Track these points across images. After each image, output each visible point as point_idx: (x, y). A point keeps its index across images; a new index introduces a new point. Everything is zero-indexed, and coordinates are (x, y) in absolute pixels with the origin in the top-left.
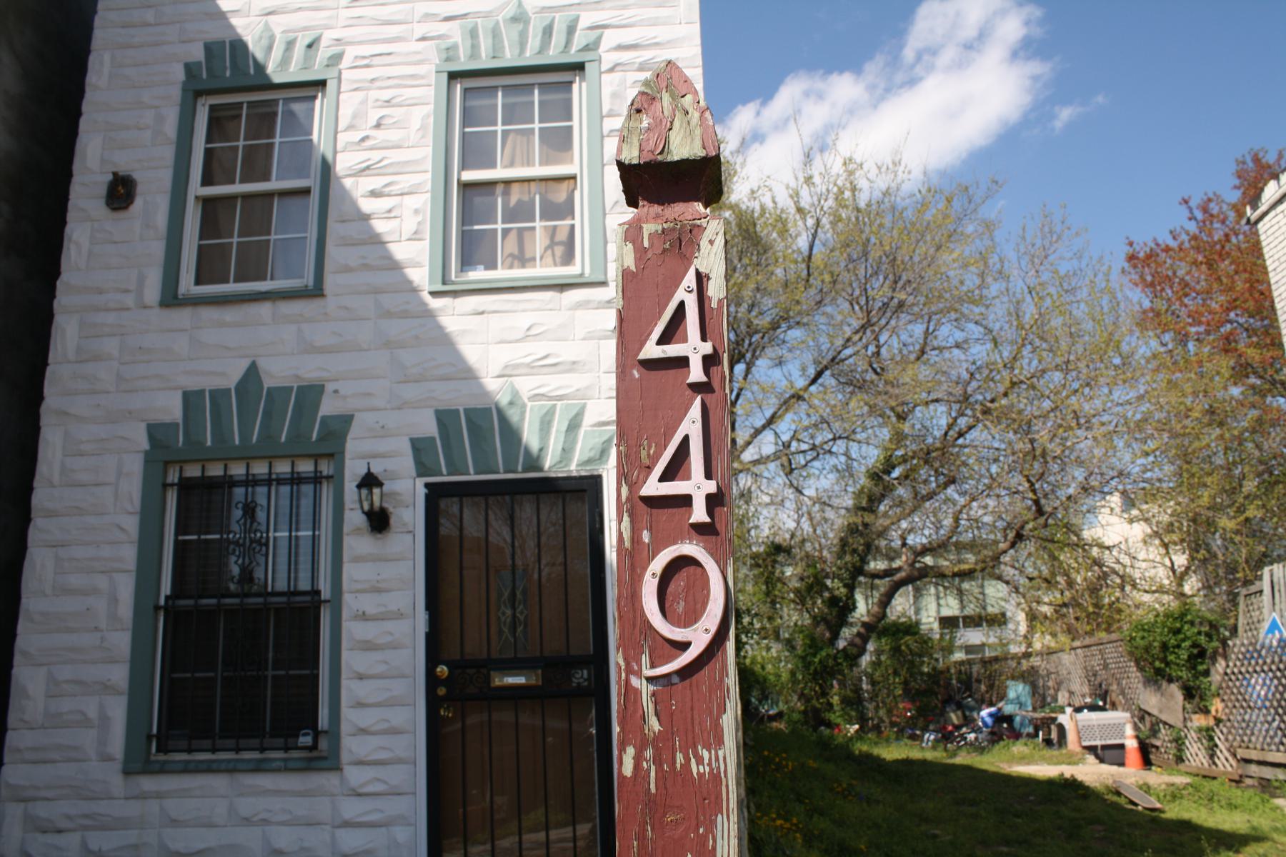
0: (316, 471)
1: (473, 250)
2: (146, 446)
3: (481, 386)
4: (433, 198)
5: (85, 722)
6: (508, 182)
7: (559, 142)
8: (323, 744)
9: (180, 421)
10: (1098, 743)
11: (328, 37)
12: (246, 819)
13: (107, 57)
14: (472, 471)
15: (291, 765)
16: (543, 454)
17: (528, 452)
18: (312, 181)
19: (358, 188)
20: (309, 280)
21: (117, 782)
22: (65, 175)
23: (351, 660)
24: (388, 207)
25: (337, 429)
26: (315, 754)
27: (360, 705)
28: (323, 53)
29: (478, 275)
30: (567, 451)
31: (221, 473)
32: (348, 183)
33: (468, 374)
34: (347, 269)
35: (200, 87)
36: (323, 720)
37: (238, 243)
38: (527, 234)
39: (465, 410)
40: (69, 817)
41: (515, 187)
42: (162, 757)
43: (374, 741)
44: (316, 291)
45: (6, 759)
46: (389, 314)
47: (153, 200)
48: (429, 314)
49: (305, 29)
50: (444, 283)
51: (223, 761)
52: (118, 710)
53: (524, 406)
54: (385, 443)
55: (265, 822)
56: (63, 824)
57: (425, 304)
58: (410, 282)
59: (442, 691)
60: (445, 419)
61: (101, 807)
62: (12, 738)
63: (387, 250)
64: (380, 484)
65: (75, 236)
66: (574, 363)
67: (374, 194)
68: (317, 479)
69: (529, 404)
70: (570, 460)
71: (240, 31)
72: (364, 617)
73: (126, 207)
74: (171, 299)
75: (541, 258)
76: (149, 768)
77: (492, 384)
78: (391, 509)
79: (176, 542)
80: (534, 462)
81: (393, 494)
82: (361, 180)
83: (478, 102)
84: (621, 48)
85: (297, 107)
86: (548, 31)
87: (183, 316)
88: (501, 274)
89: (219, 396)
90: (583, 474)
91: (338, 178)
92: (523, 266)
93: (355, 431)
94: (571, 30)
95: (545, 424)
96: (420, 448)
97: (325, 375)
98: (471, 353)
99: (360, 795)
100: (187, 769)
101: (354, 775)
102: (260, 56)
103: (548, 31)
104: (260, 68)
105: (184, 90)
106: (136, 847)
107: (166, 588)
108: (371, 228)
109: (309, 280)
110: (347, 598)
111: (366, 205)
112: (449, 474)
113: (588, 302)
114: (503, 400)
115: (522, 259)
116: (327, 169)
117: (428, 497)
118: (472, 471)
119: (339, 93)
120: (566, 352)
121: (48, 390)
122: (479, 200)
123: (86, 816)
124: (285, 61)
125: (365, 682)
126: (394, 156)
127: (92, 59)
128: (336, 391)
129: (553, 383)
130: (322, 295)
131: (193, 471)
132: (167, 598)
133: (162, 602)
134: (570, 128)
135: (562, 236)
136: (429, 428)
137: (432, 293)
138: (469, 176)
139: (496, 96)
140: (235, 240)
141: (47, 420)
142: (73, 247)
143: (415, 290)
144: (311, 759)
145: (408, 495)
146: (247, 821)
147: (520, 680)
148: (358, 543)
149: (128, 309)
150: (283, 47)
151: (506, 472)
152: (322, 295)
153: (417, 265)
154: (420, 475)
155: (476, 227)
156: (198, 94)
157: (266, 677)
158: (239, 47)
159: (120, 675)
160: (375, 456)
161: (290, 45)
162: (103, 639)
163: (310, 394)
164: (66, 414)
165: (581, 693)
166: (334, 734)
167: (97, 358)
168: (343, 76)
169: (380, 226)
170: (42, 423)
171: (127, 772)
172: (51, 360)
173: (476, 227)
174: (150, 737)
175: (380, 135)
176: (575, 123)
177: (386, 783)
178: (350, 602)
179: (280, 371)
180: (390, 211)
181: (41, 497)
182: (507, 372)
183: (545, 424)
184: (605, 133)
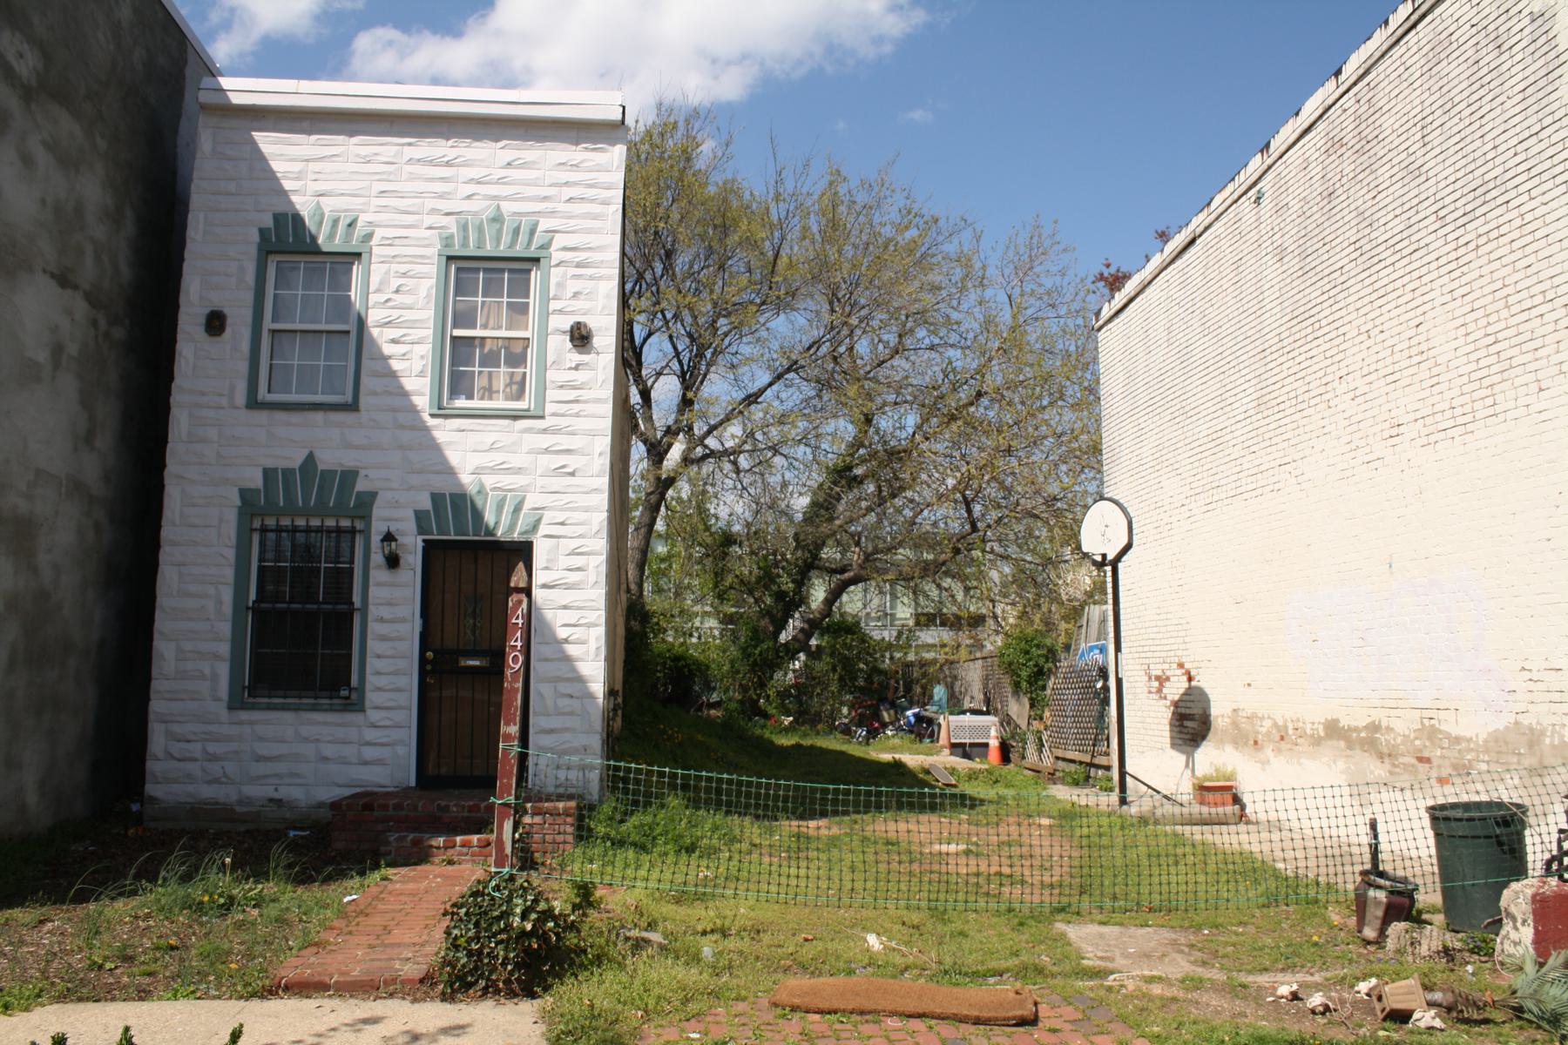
3: (458, 480)
6: (483, 338)
18: (352, 326)
19: (380, 335)
20: (349, 398)
21: (223, 713)
22: (175, 308)
23: (372, 645)
25: (366, 502)
27: (378, 673)
29: (461, 403)
32: (375, 332)
33: (450, 472)
34: (375, 393)
36: (354, 681)
43: (387, 695)
44: (353, 407)
46: (402, 427)
48: (426, 430)
52: (224, 670)
54: (397, 513)
55: (318, 740)
59: (429, 667)
60: (437, 499)
62: (155, 685)
67: (394, 341)
72: (381, 620)
76: (244, 707)
77: (466, 479)
80: (490, 533)
84: (565, 249)
86: (516, 231)
87: (262, 416)
88: (476, 403)
89: (288, 473)
93: (378, 503)
96: (420, 516)
101: (373, 715)
102: (313, 229)
103: (516, 231)
104: (314, 239)
105: (260, 250)
107: (253, 596)
109: (349, 398)
110: (372, 608)
111: (387, 349)
114: (472, 490)
115: (489, 392)
116: (361, 323)
120: (516, 461)
124: (331, 236)
126: (409, 315)
129: (506, 481)
135: (518, 378)
136: (426, 504)
142: (183, 362)
143: (413, 410)
147: (477, 663)
153: (422, 394)
154: (420, 533)
156: (270, 252)
158: (298, 220)
159: (225, 649)
161: (336, 222)
163: (349, 476)
166: (361, 690)
169: (395, 365)
171: (231, 708)
175: (399, 299)
178: (374, 611)
179: (329, 459)
181: (166, 532)
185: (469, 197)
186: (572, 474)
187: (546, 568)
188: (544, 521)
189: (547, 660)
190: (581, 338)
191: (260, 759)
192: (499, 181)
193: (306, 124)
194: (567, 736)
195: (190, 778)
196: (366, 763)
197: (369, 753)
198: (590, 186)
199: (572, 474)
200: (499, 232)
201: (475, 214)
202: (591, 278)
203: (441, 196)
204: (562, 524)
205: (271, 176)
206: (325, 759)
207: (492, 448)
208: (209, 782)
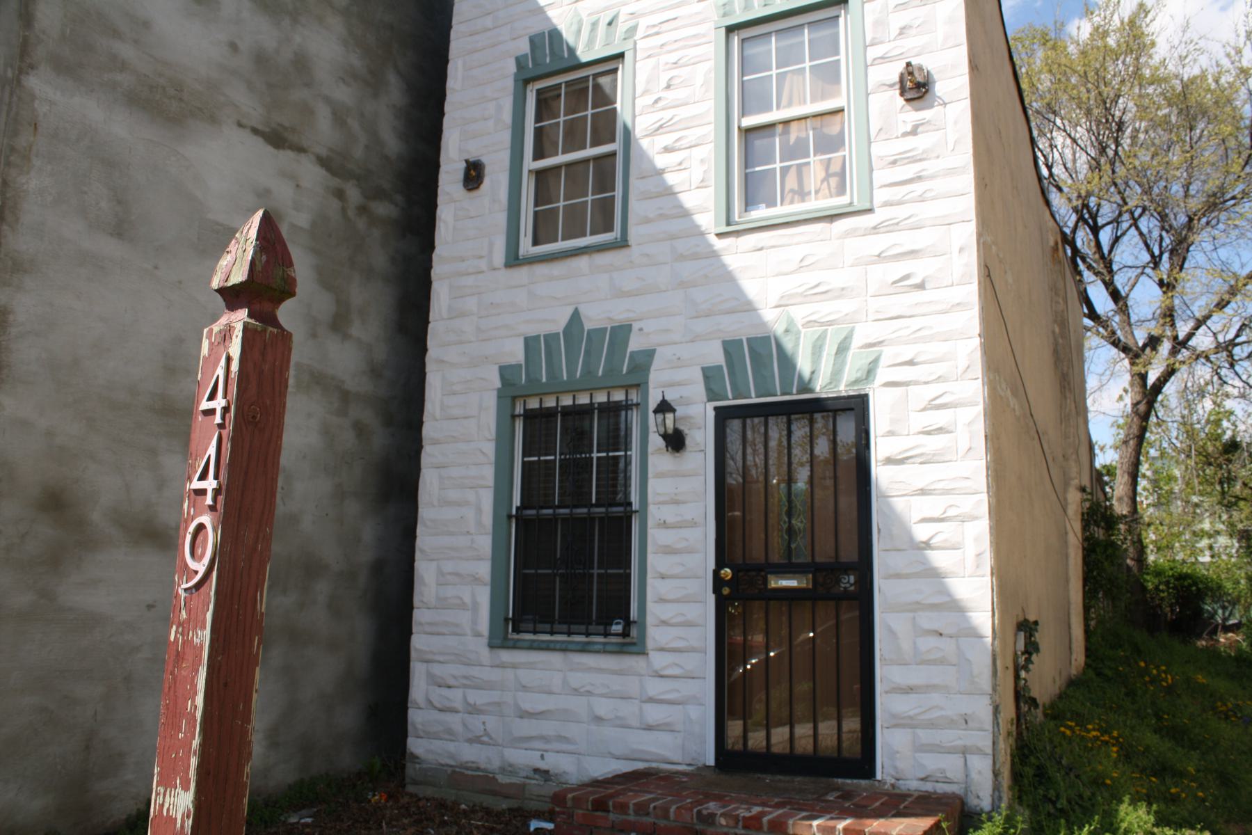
0: (627, 400)
2: (498, 384)
3: (759, 317)
4: (716, 147)
5: (462, 606)
6: (786, 123)
7: (829, 76)
8: (634, 632)
9: (523, 362)
11: (625, 11)
12: (576, 690)
13: (460, 63)
14: (753, 395)
15: (609, 648)
16: (815, 376)
17: (800, 377)
21: (485, 652)
23: (655, 562)
24: (678, 161)
25: (643, 362)
26: (627, 640)
27: (662, 600)
28: (621, 28)
29: (761, 213)
30: (836, 374)
31: (554, 404)
33: (748, 307)
34: (647, 221)
35: (529, 76)
36: (634, 613)
37: (564, 206)
38: (804, 169)
39: (748, 340)
40: (454, 677)
41: (794, 126)
42: (516, 636)
45: (414, 630)
46: (682, 258)
48: (714, 255)
49: (607, 8)
50: (728, 224)
51: (558, 642)
52: (484, 597)
53: (799, 332)
55: (589, 693)
56: (452, 682)
57: (711, 246)
58: (698, 227)
59: (726, 591)
61: (475, 672)
63: (677, 200)
64: (673, 411)
65: (443, 216)
66: (843, 289)
67: (667, 150)
68: (628, 406)
69: (803, 331)
70: (839, 381)
71: (555, 21)
72: (664, 525)
73: (477, 187)
74: (514, 260)
75: (817, 192)
78: (686, 431)
79: (524, 463)
80: (805, 387)
81: (686, 418)
82: (656, 138)
83: (754, 50)
85: (603, 81)
87: (522, 273)
89: (551, 339)
90: (852, 393)
91: (637, 140)
92: (803, 201)
95: (817, 350)
96: (710, 375)
97: (631, 315)
98: (751, 288)
99: (662, 676)
100: (532, 647)
101: (658, 660)
104: (572, 51)
106: (498, 704)
107: (517, 501)
108: (664, 181)
110: (652, 509)
111: (660, 161)
112: (734, 398)
113: (855, 230)
114: (779, 329)
115: (802, 194)
116: (627, 133)
117: (716, 417)
118: (753, 395)
119: (635, 61)
120: (835, 279)
122: (759, 143)
123: (466, 677)
124: (591, 42)
125: (667, 581)
126: (683, 113)
127: (450, 67)
128: (641, 330)
130: (628, 246)
131: (533, 404)
132: (518, 508)
133: (514, 512)
134: (838, 61)
135: (835, 168)
137: (717, 235)
138: (748, 122)
139: (803, 34)
140: (561, 204)
141: (430, 367)
143: (702, 234)
144: (624, 644)
146: (576, 692)
147: (793, 583)
148: (660, 460)
149: (482, 272)
150: (589, 28)
151: (783, 394)
152: (628, 246)
153: (704, 210)
154: (709, 400)
155: (757, 169)
156: (527, 82)
157: (592, 575)
158: (555, 35)
159: (484, 570)
160: (672, 385)
161: (594, 25)
162: (472, 541)
163: (621, 332)
164: (443, 361)
165: (846, 596)
168: (638, 47)
169: (671, 179)
170: (427, 370)
171: (492, 646)
172: (431, 319)
173: (757, 169)
174: (507, 620)
176: (842, 57)
177: (682, 668)
179: (596, 316)
180: (680, 164)
182: (782, 303)
183: (817, 350)
184: (869, 62)
186: (921, 286)
187: (891, 433)
188: (882, 363)
189: (898, 576)
190: (916, 88)
191: (524, 715)
194: (936, 698)
195: (450, 734)
196: (649, 728)
197: (655, 714)
199: (921, 286)
204: (911, 363)
206: (598, 719)
207: (802, 266)
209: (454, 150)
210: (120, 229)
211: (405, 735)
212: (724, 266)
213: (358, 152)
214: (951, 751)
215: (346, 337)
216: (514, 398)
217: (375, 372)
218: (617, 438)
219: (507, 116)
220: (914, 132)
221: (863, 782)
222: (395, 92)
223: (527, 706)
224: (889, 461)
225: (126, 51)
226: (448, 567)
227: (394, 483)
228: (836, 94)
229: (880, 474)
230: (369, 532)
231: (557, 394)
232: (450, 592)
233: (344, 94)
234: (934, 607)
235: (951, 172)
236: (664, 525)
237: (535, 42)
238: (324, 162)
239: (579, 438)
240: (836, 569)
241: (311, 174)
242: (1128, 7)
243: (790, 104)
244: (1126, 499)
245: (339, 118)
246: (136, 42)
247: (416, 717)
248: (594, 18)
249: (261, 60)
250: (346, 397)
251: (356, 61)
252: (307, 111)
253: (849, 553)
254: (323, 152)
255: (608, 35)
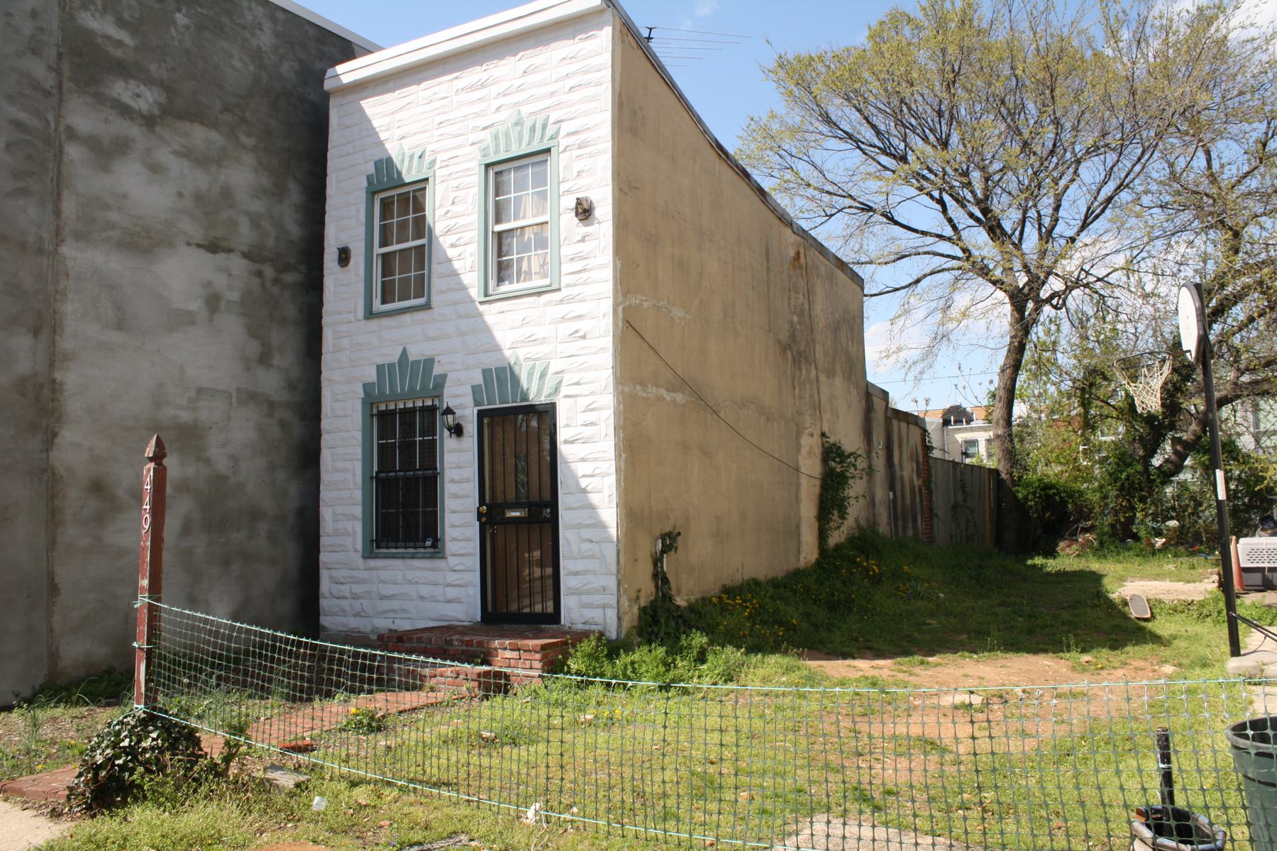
1: (503, 271)
2: (362, 395)
5: (347, 534)
6: (522, 228)
10: (1266, 565)
11: (429, 148)
21: (360, 561)
25: (441, 381)
27: (453, 526)
28: (428, 159)
29: (506, 287)
30: (540, 390)
33: (497, 349)
34: (443, 292)
46: (460, 317)
47: (357, 259)
48: (480, 315)
49: (418, 146)
50: (486, 295)
55: (417, 583)
59: (484, 519)
61: (355, 573)
64: (454, 413)
72: (453, 481)
74: (370, 314)
77: (507, 353)
80: (525, 397)
81: (462, 417)
84: (569, 134)
87: (374, 324)
89: (391, 366)
94: (544, 127)
95: (531, 374)
96: (476, 390)
100: (387, 557)
101: (452, 561)
104: (399, 174)
107: (375, 469)
111: (451, 253)
116: (430, 231)
121: (323, 368)
124: (410, 169)
131: (383, 407)
138: (498, 228)
140: (397, 277)
141: (324, 384)
143: (473, 301)
145: (468, 415)
146: (410, 582)
154: (476, 405)
156: (374, 193)
158: (389, 161)
159: (358, 511)
161: (412, 157)
163: (429, 362)
165: (545, 521)
167: (341, 350)
171: (364, 557)
175: (455, 209)
179: (415, 353)
181: (324, 424)
183: (531, 374)
185: (498, 109)
186: (584, 337)
187: (567, 426)
188: (564, 383)
189: (571, 509)
190: (584, 212)
191: (383, 598)
192: (520, 89)
193: (391, 85)
194: (590, 577)
195: (343, 613)
196: (449, 601)
197: (451, 593)
198: (586, 72)
199: (584, 337)
200: (521, 134)
201: (503, 123)
202: (591, 155)
203: (478, 115)
204: (577, 384)
205: (373, 133)
206: (422, 598)
207: (524, 323)
208: (355, 615)
209: (333, 239)
210: (120, 325)
211: (318, 615)
212: (484, 322)
213: (270, 243)
214: (597, 607)
215: (270, 366)
216: (372, 404)
217: (291, 386)
218: (430, 429)
219: (362, 217)
220: (583, 240)
221: (555, 626)
222: (295, 194)
223: (384, 593)
224: (566, 442)
225: (114, 216)
226: (339, 510)
227: (307, 458)
228: (544, 212)
229: (563, 449)
230: (294, 489)
231: (396, 401)
232: (340, 525)
233: (258, 206)
234: (588, 526)
235: (601, 266)
236: (453, 481)
237: (378, 164)
238: (246, 255)
239: (408, 428)
240: (542, 505)
241: (238, 265)
242: (959, 4)
243: (524, 217)
244: (1001, 422)
245: (255, 223)
246: (120, 209)
247: (324, 603)
248: (410, 152)
249: (199, 198)
250: (272, 405)
251: (265, 181)
252: (233, 224)
253: (547, 496)
254: (246, 249)
255: (420, 165)
